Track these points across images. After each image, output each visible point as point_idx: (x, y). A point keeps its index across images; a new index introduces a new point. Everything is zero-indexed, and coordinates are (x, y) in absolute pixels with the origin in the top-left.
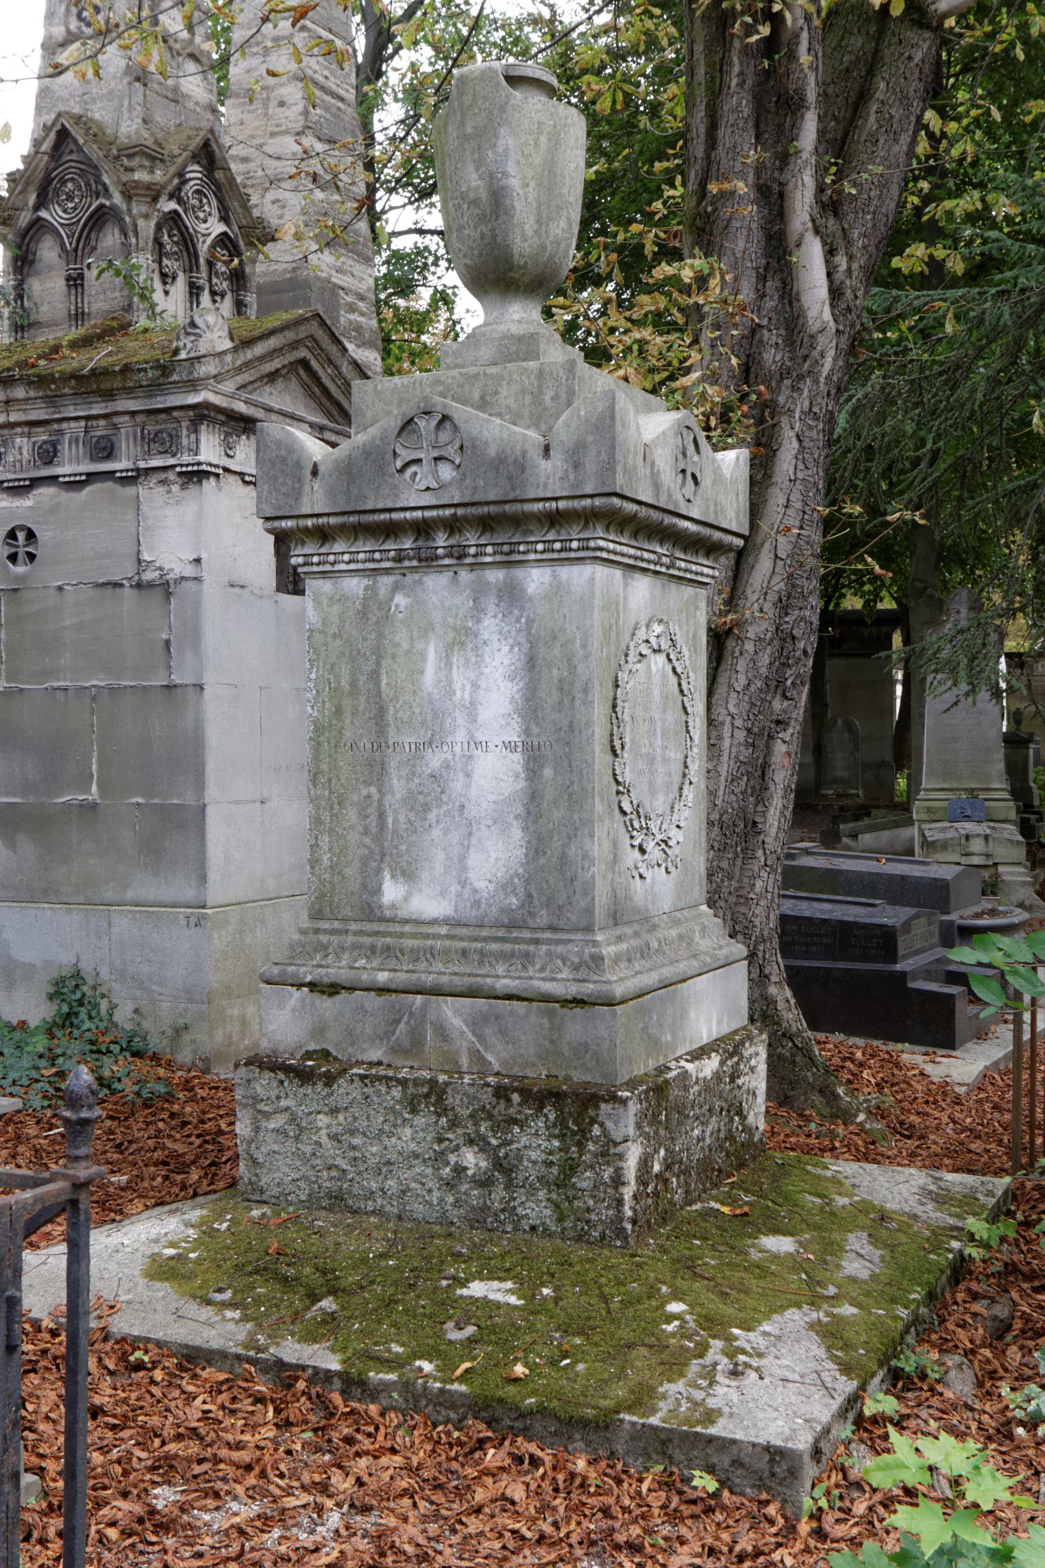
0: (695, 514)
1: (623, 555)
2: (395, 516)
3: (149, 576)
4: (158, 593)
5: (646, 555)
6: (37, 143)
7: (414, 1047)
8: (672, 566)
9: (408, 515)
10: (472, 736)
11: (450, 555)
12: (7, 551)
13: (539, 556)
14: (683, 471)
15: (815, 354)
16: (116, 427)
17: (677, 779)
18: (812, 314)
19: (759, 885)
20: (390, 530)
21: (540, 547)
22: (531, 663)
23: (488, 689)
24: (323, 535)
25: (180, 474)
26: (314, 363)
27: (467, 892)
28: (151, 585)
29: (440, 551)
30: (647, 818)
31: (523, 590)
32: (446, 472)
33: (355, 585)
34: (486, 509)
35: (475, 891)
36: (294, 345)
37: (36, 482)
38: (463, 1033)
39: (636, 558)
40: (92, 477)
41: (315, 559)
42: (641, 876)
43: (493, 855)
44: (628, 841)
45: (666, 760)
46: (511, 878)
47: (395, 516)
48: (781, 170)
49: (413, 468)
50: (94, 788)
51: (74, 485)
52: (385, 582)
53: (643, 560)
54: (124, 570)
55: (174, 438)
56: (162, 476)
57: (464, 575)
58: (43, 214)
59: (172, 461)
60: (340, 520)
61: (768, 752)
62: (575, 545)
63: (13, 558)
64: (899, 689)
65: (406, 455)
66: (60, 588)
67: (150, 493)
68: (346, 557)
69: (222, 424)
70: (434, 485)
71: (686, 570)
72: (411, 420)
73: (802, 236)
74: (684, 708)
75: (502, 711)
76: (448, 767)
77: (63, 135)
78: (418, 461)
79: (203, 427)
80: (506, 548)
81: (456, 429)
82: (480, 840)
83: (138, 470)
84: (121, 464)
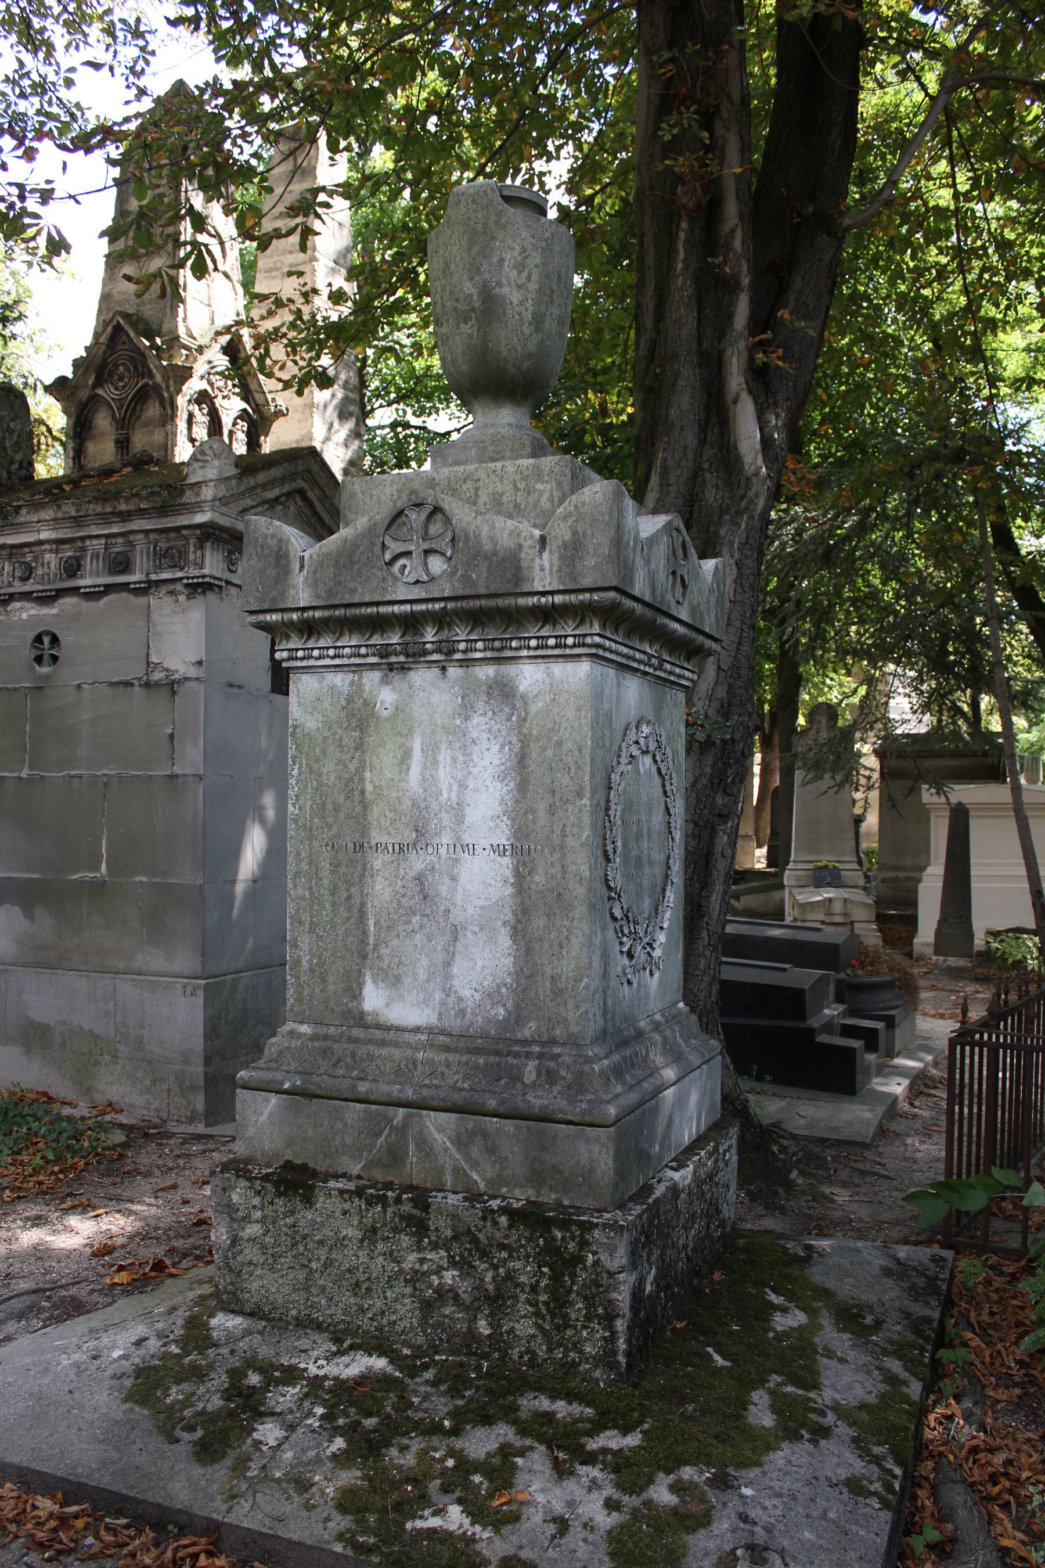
0: (684, 616)
1: (618, 654)
2: (383, 609)
3: (157, 676)
4: (165, 692)
5: (638, 655)
6: (97, 335)
7: (395, 1156)
8: (660, 668)
9: (396, 609)
10: (459, 838)
11: (439, 651)
12: (35, 653)
13: (532, 653)
14: (674, 573)
15: (751, 494)
16: (131, 544)
17: (659, 879)
18: (747, 460)
19: (703, 962)
20: (379, 624)
21: (533, 643)
22: (522, 760)
23: (477, 790)
24: (309, 629)
25: (187, 585)
26: (310, 494)
27: (452, 999)
28: (157, 685)
29: (428, 646)
30: (636, 923)
31: (515, 688)
32: (437, 565)
33: (340, 680)
34: (478, 603)
35: (460, 999)
36: (292, 477)
37: (60, 593)
38: (446, 1150)
39: (629, 657)
40: (109, 589)
41: (300, 654)
42: (629, 982)
43: (480, 963)
44: (617, 948)
45: (651, 863)
46: (498, 987)
47: (383, 609)
48: (720, 340)
49: (402, 561)
50: (104, 866)
51: (93, 595)
52: (373, 677)
53: (635, 660)
54: (134, 671)
55: (183, 554)
56: (171, 587)
57: (453, 671)
58: (100, 392)
59: (179, 574)
60: (326, 613)
61: (711, 843)
62: (570, 641)
63: (39, 660)
64: (756, 781)
65: (395, 547)
66: (79, 686)
67: (160, 604)
68: (331, 652)
69: (226, 542)
70: (425, 578)
71: (671, 673)
72: (401, 513)
73: (738, 395)
74: (667, 809)
75: (491, 813)
76: (433, 869)
77: (118, 329)
78: (407, 554)
79: (208, 545)
80: (497, 644)
81: (448, 520)
82: (466, 947)
83: (149, 582)
84: (135, 578)
